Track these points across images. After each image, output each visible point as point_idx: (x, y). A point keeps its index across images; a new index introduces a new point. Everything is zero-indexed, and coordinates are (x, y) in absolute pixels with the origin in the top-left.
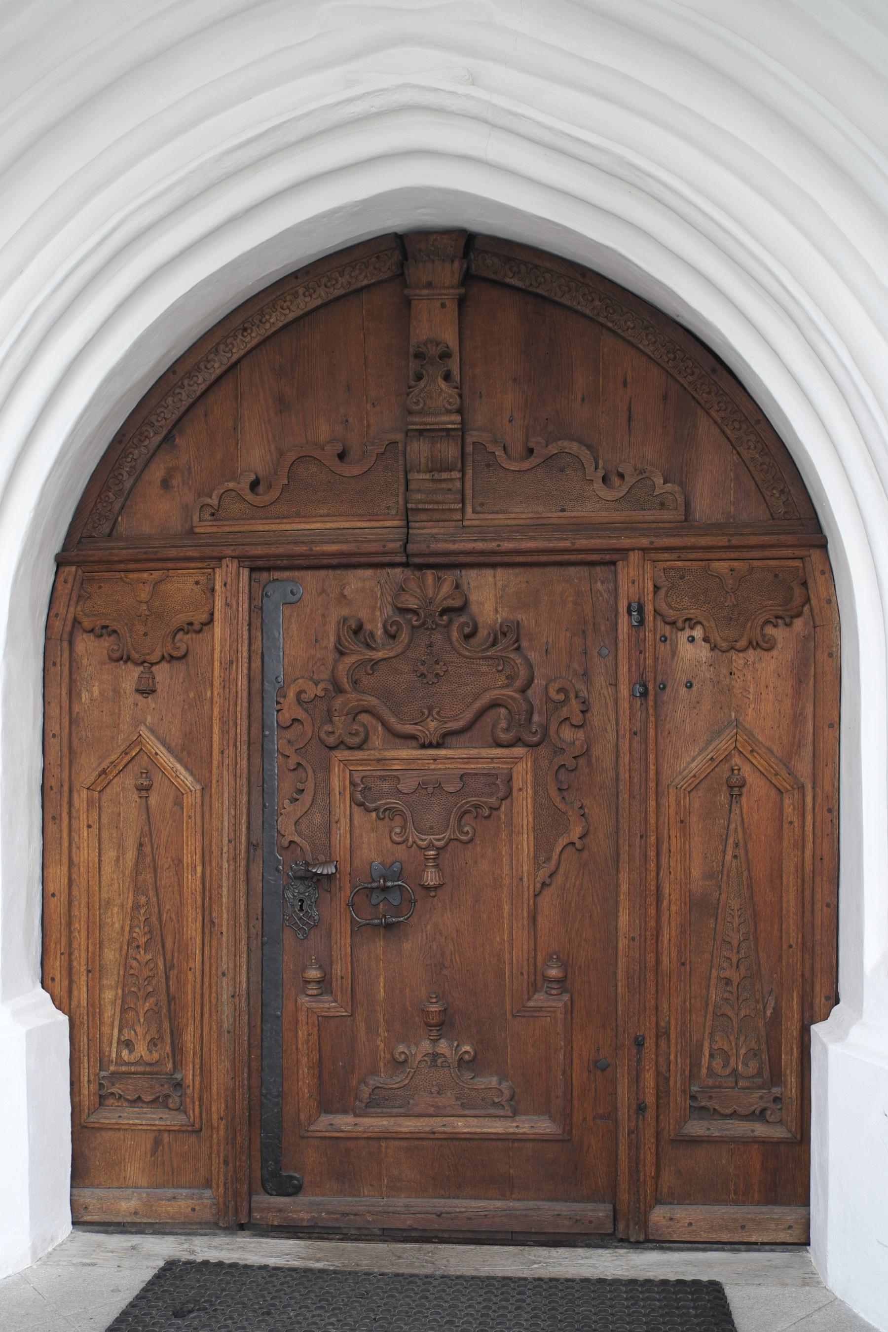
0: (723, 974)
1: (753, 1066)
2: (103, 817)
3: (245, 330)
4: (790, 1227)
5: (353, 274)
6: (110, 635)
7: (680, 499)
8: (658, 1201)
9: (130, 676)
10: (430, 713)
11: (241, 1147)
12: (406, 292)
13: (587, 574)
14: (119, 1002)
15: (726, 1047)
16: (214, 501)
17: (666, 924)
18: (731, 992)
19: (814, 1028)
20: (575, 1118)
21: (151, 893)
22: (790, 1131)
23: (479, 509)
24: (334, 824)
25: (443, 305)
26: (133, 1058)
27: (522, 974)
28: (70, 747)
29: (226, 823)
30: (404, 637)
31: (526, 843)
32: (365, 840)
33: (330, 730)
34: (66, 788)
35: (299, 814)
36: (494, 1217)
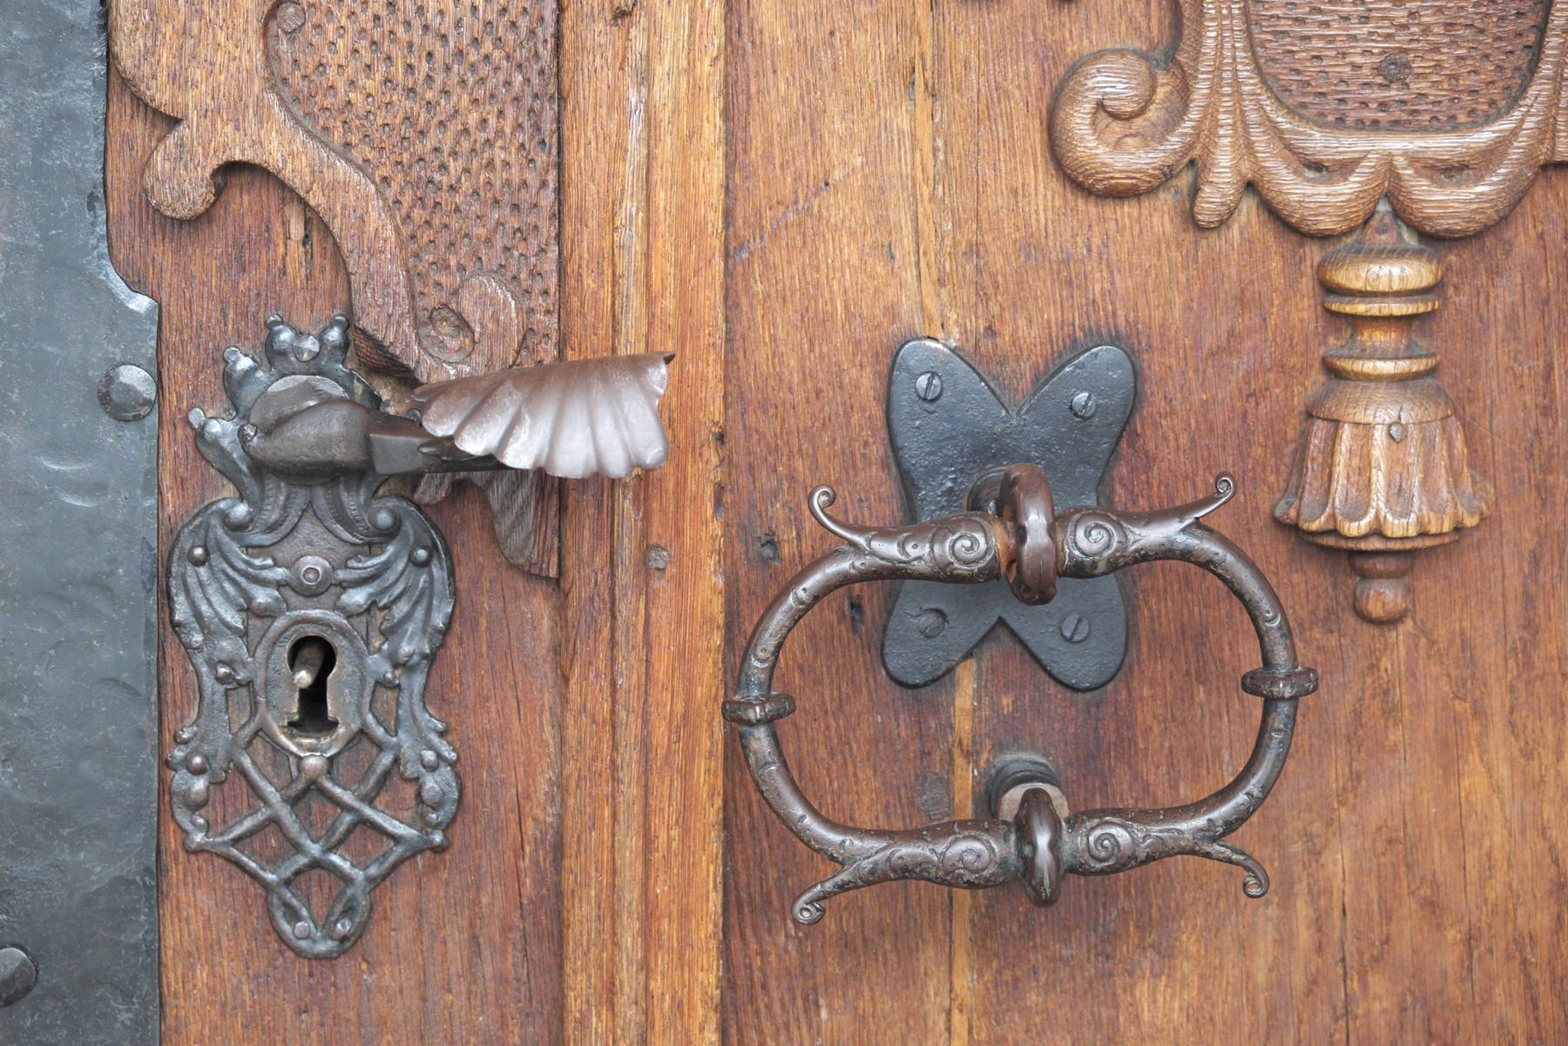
24: (599, 32)
32: (846, 160)
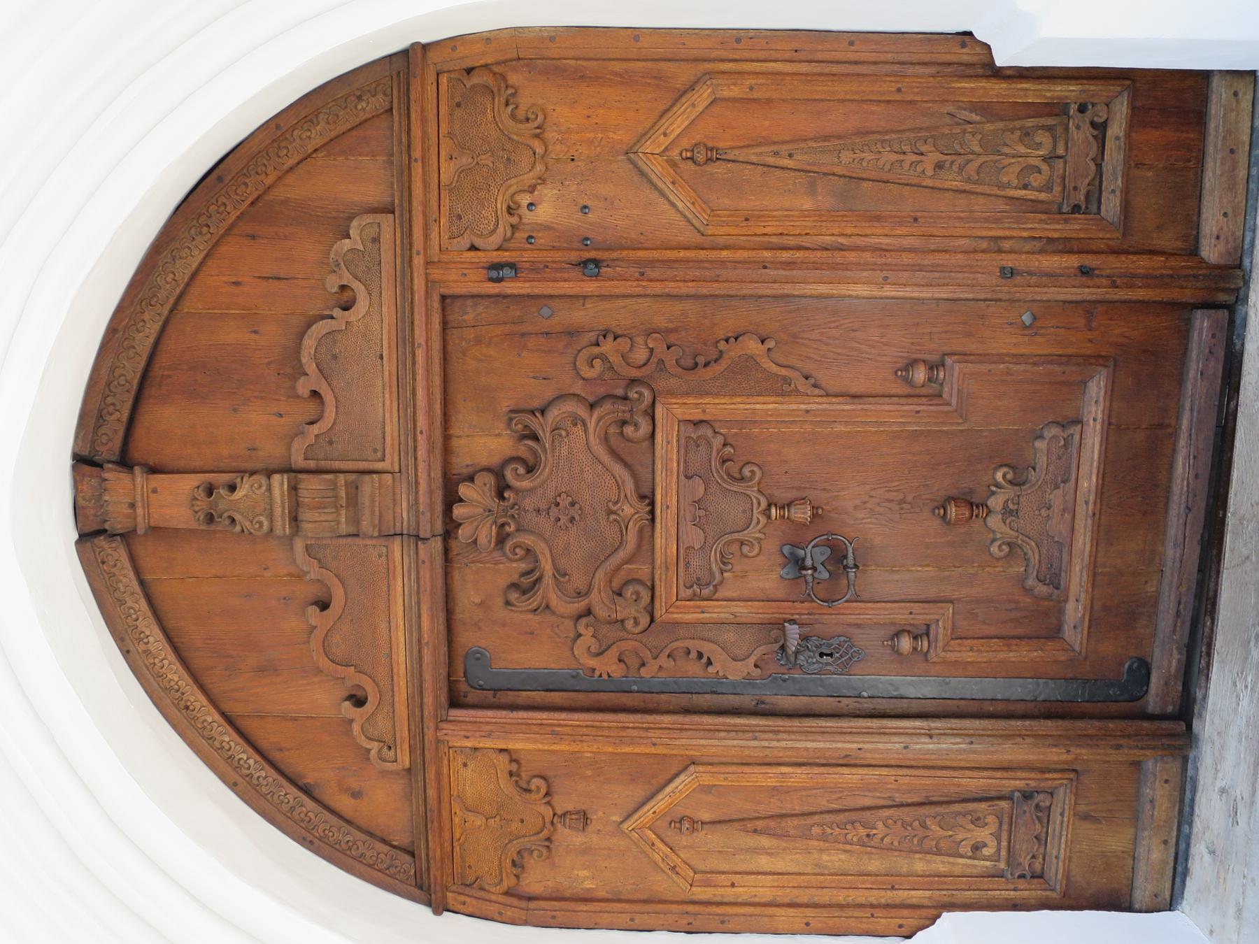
0: (930, 172)
1: (1043, 138)
2: (722, 869)
3: (187, 708)
4: (1236, 94)
5: (122, 589)
6: (522, 857)
7: (368, 219)
8: (1194, 252)
9: (567, 837)
10: (614, 513)
11: (1100, 729)
12: (141, 531)
13: (455, 331)
14: (928, 857)
15: (1017, 169)
16: (374, 746)
17: (867, 239)
18: (952, 163)
19: (999, 63)
20: (1089, 352)
21: (809, 821)
22: (1120, 93)
23: (379, 454)
25: (155, 491)
26: (992, 844)
27: (918, 412)
28: (645, 902)
29: (735, 742)
30: (528, 540)
31: (765, 406)
33: (632, 621)
34: (691, 908)
35: (725, 656)
36: (1197, 448)
